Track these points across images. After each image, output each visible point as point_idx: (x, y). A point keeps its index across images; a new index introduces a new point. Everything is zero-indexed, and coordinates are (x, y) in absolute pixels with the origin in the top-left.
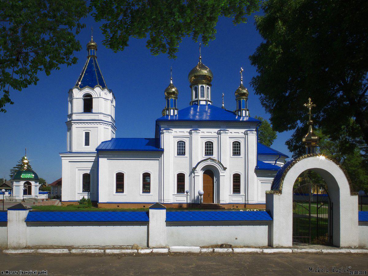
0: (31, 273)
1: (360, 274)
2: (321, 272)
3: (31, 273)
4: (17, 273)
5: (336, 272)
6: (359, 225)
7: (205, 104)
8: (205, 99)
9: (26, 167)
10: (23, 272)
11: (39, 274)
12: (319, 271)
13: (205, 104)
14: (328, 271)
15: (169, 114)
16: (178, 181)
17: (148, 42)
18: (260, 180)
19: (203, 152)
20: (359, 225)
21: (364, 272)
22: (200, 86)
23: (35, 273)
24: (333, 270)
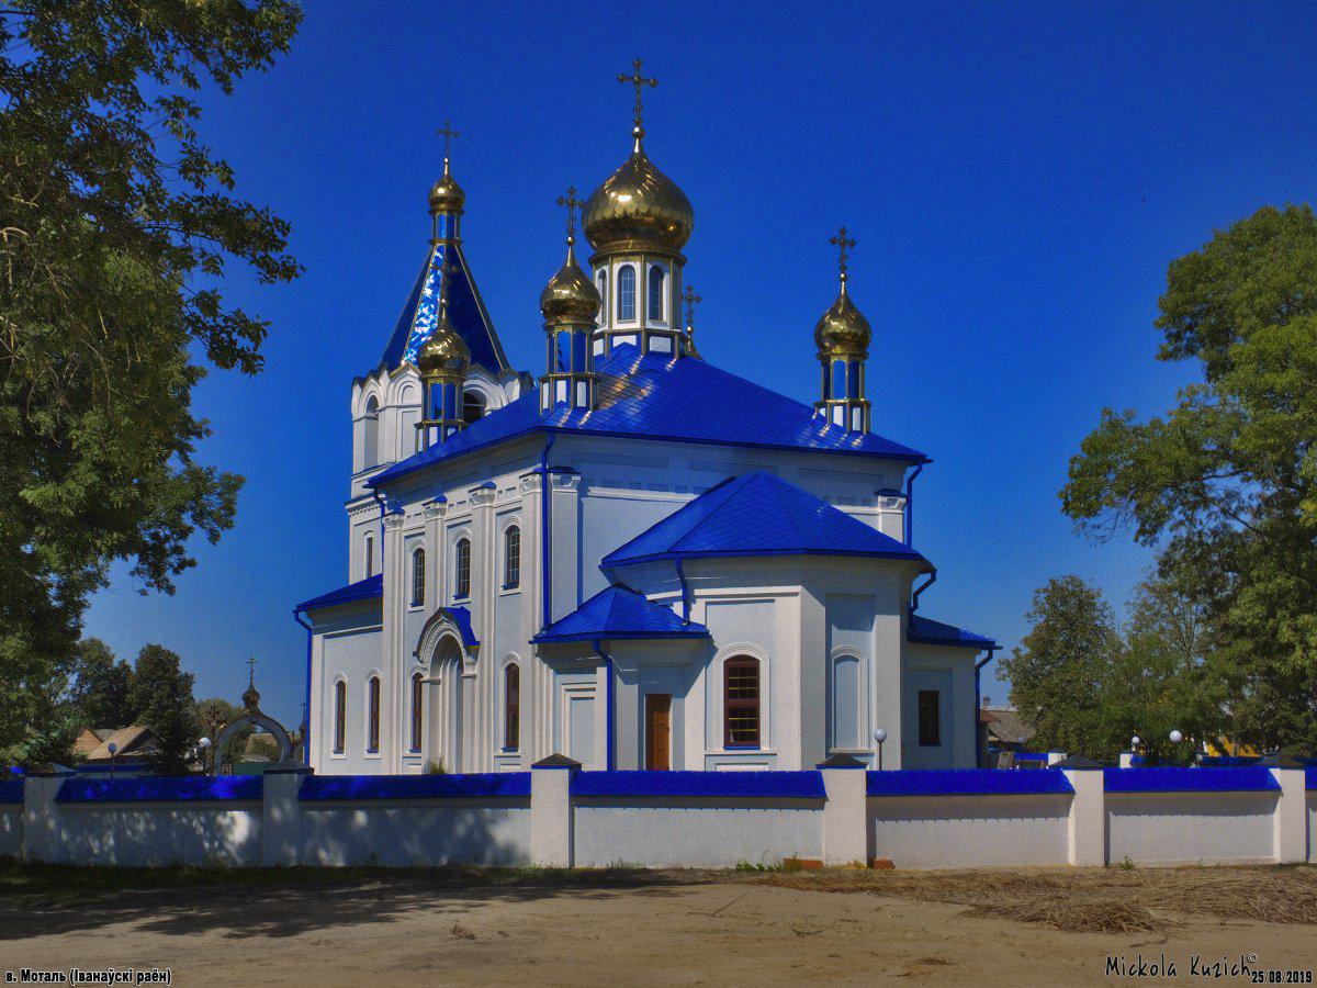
0: (111, 979)
1: (1289, 981)
2: (1148, 973)
3: (111, 979)
4: (61, 976)
5: (1169, 974)
6: (529, 807)
7: (668, 350)
8: (637, 325)
9: (281, 807)
10: (82, 975)
11: (139, 980)
12: (1141, 973)
13: (668, 350)
14: (1174, 971)
15: (848, 411)
16: (754, 712)
17: (289, 278)
18: (569, 687)
19: (319, 677)
20: (529, 807)
21: (1302, 973)
22: (617, 267)
23: (125, 976)
24: (1193, 967)
